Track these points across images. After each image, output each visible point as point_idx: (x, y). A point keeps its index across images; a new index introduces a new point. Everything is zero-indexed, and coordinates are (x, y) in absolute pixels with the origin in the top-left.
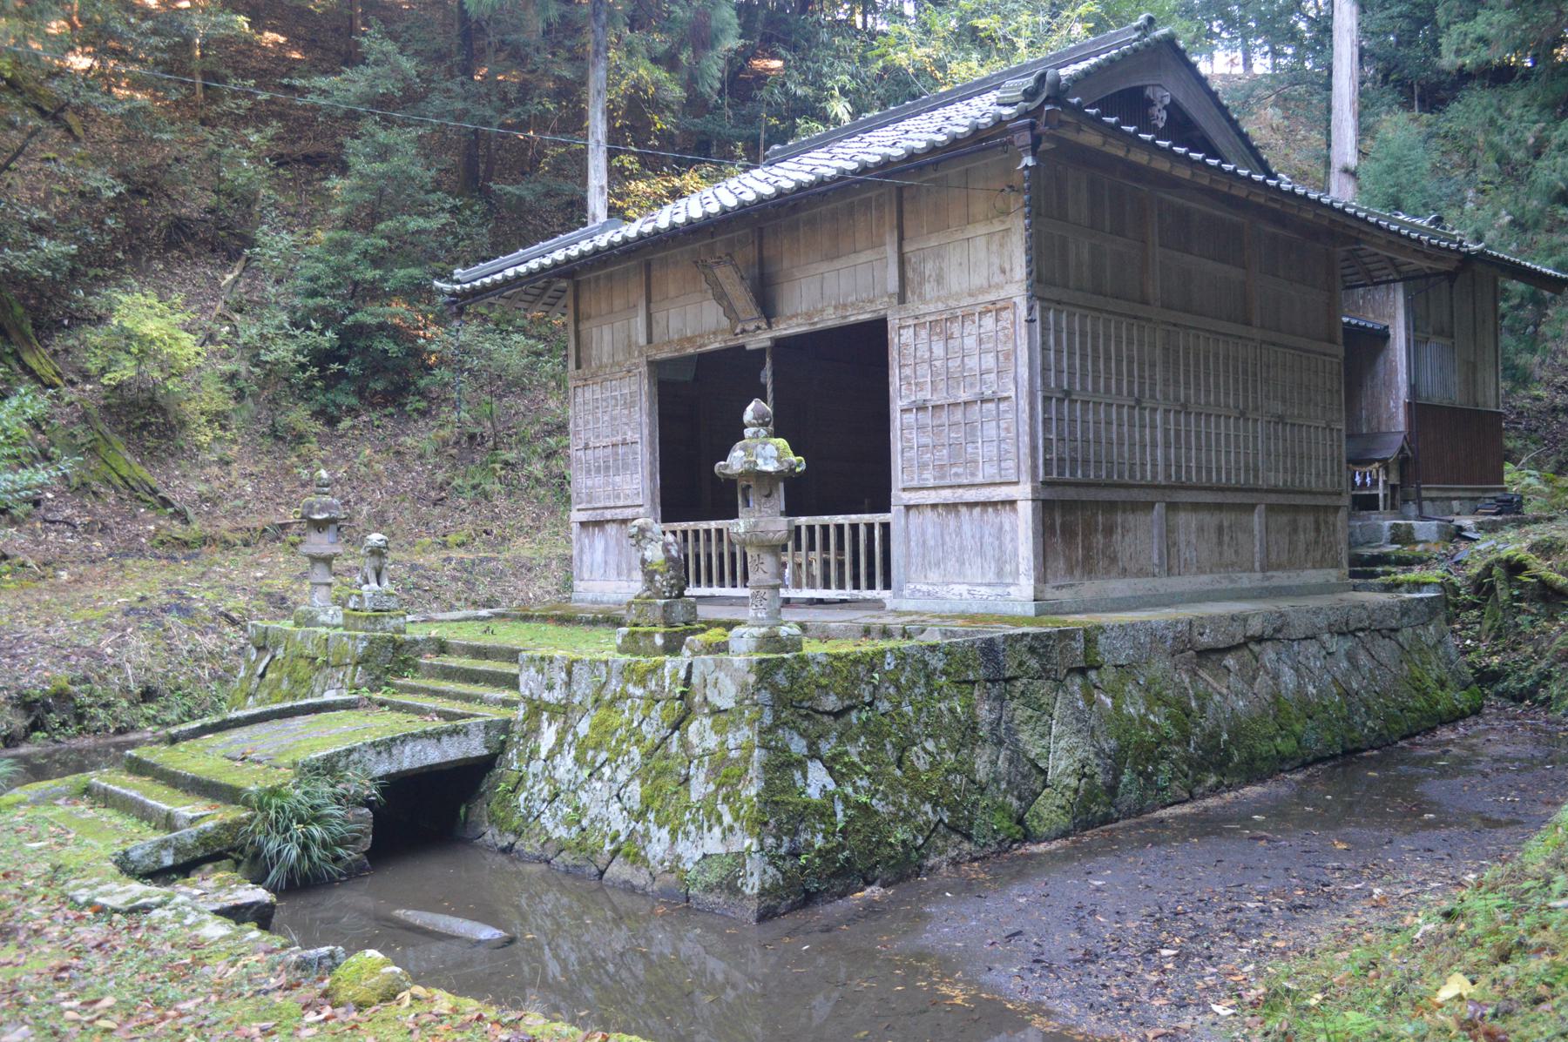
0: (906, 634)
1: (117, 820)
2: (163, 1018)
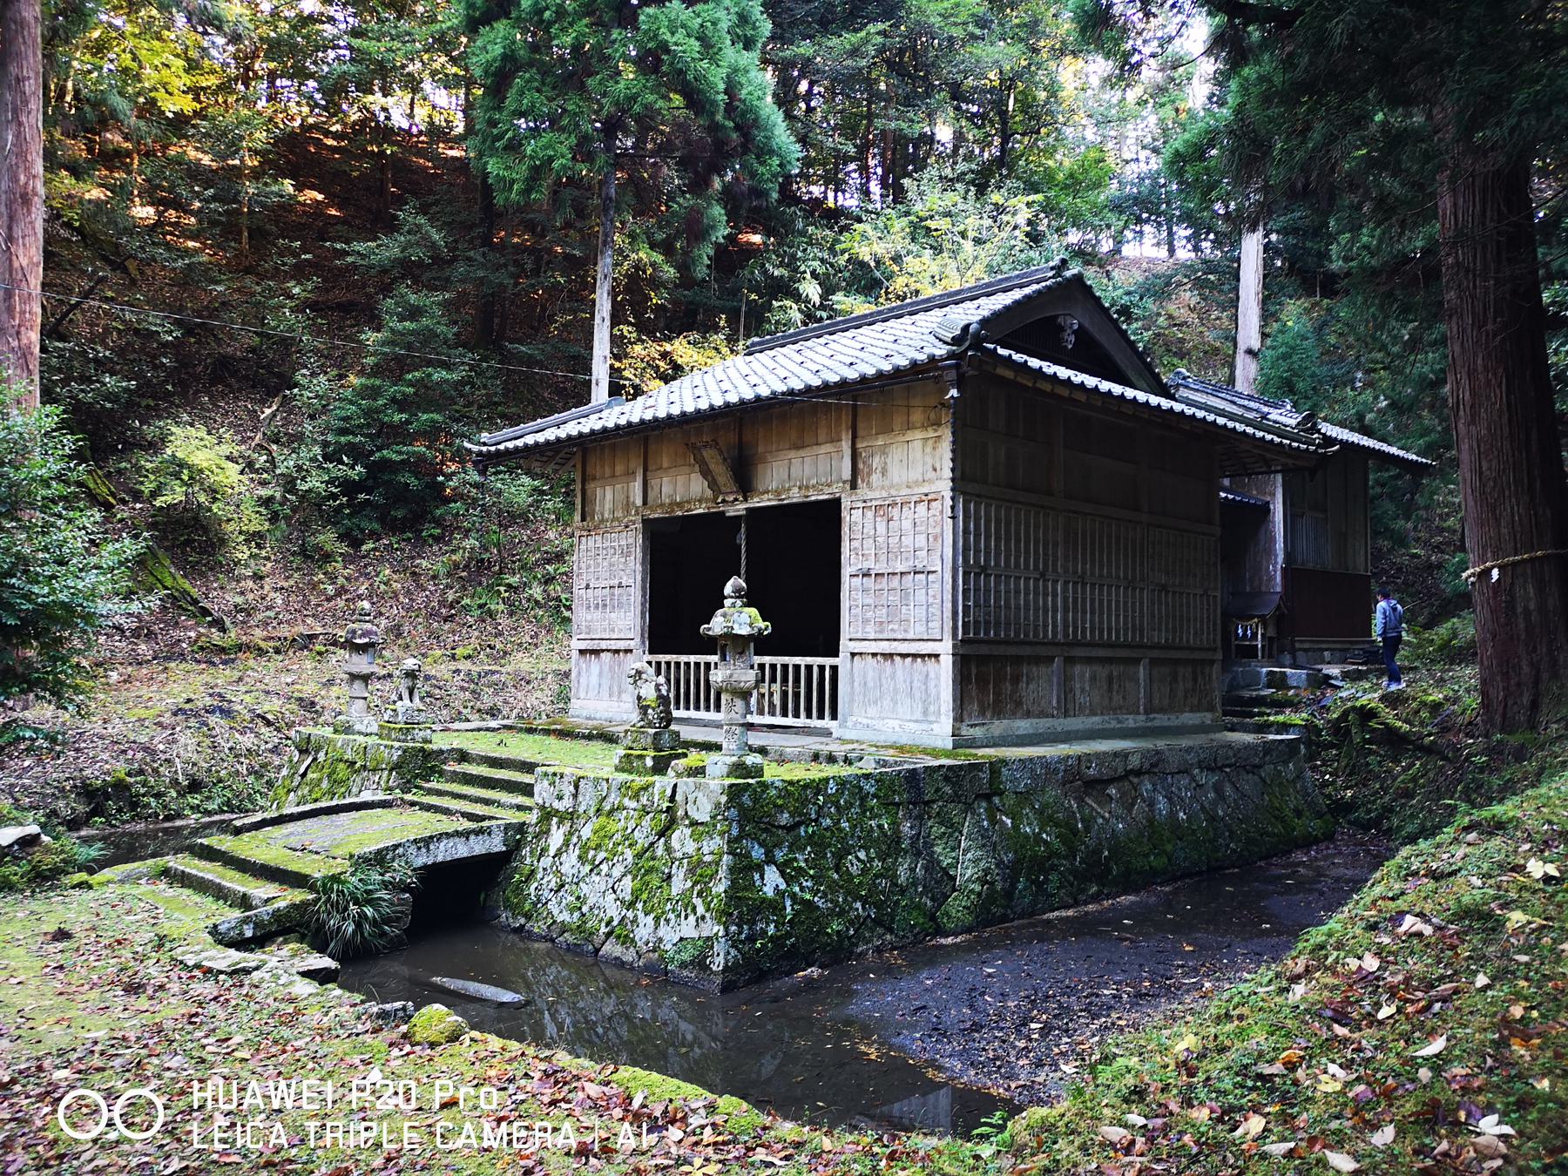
1: (197, 898)
2: (284, 1052)
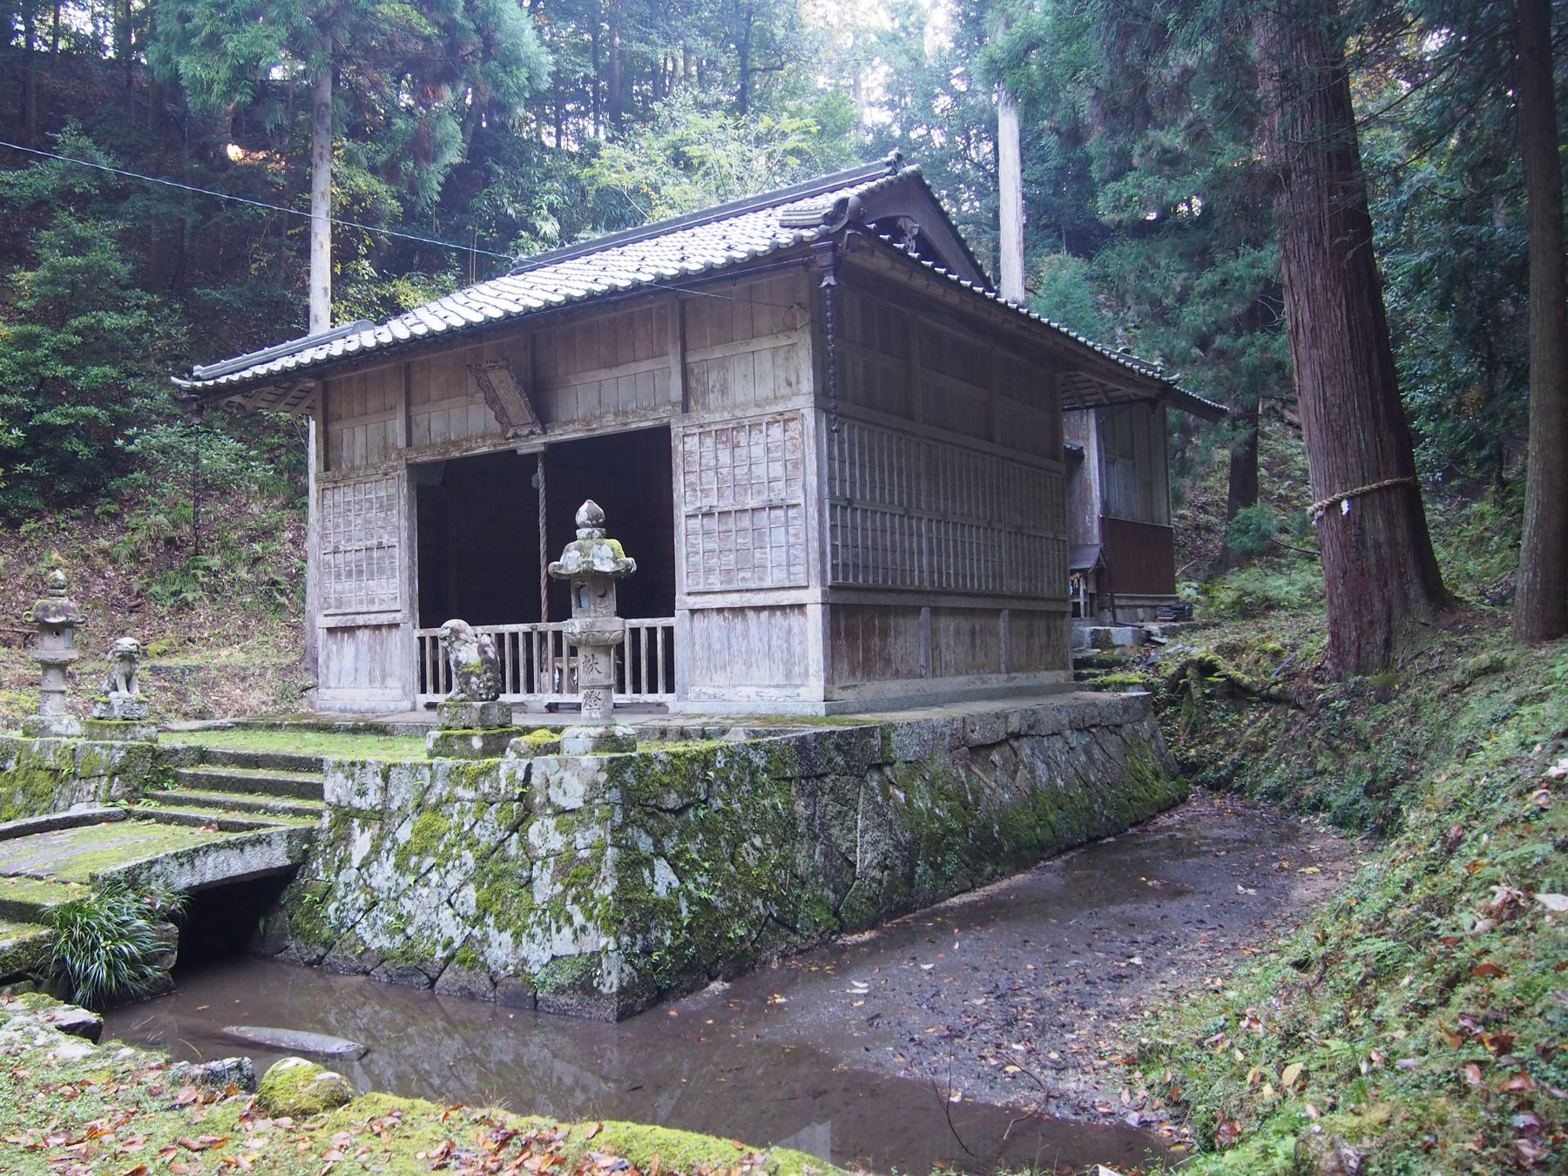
0: (705, 735)
